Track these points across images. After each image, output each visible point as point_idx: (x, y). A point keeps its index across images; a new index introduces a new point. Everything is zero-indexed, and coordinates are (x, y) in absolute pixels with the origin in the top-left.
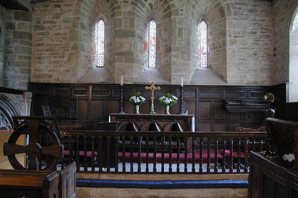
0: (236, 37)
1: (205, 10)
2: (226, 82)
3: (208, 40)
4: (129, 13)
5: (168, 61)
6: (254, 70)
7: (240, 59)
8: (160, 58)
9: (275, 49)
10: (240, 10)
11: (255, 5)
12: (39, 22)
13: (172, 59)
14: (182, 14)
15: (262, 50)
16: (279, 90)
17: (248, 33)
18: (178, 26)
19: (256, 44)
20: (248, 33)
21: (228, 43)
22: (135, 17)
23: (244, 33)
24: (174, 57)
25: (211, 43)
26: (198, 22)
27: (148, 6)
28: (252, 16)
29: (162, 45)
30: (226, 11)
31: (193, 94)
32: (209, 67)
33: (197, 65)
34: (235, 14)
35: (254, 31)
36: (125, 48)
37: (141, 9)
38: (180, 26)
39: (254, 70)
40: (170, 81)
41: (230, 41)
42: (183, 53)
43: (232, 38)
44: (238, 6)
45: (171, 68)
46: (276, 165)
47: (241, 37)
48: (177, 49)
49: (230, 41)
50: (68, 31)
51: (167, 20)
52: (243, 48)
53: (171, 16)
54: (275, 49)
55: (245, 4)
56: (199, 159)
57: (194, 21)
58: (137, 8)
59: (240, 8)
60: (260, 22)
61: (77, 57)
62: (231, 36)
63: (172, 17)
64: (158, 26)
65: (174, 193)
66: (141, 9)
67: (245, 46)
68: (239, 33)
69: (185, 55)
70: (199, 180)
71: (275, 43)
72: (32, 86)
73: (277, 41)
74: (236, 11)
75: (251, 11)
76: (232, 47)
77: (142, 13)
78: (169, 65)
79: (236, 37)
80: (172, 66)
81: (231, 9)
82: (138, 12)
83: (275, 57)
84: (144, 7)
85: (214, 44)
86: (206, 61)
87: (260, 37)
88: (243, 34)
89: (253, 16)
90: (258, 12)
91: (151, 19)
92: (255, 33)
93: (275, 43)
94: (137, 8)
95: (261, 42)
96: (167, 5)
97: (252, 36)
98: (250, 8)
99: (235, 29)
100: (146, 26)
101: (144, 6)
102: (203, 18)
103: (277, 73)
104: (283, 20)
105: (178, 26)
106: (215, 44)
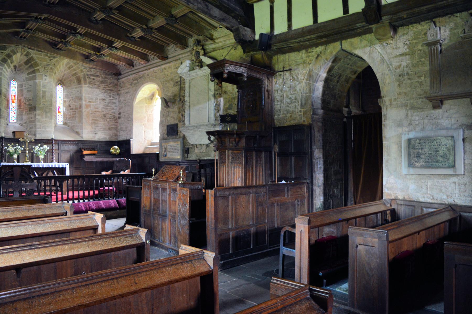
0: (90, 102)
1: (63, 76)
2: (82, 137)
3: (64, 102)
5: (32, 118)
6: (104, 129)
7: (93, 120)
8: (22, 115)
9: (120, 114)
10: (94, 81)
11: (106, 78)
13: (37, 117)
14: (45, 79)
15: (110, 113)
16: (125, 145)
17: (100, 100)
18: (42, 89)
19: (106, 109)
20: (100, 100)
21: (84, 106)
22: (2, 77)
24: (39, 115)
25: (67, 104)
26: (56, 86)
27: (12, 67)
28: (103, 86)
29: (25, 103)
30: (82, 80)
32: (65, 124)
33: (54, 125)
34: (90, 83)
35: (104, 98)
37: (7, 70)
38: (44, 90)
39: (104, 129)
40: (35, 135)
41: (86, 105)
42: (46, 112)
43: (87, 103)
44: (92, 77)
45: (35, 125)
46: (249, 255)
47: (94, 102)
48: (41, 109)
49: (86, 105)
51: (31, 82)
52: (96, 111)
53: (36, 79)
54: (120, 114)
55: (97, 76)
58: (4, 69)
59: (94, 79)
60: (109, 91)
62: (86, 101)
63: (37, 81)
65: (3, 215)
66: (7, 70)
67: (97, 110)
68: (92, 99)
69: (49, 115)
71: (120, 109)
73: (122, 107)
74: (91, 81)
75: (102, 82)
76: (87, 110)
77: (7, 73)
78: (34, 121)
79: (90, 102)
80: (37, 123)
81: (87, 79)
82: (4, 72)
83: (120, 119)
84: (9, 68)
85: (70, 106)
86: (62, 119)
87: (109, 103)
88: (96, 100)
89: (104, 86)
90: (107, 83)
92: (103, 100)
93: (120, 109)
94: (4, 69)
95: (109, 107)
96: (32, 70)
97: (102, 102)
98: (101, 79)
99: (90, 96)
100: (9, 85)
101: (9, 67)
102: (61, 82)
103: (122, 132)
104: (127, 93)
105: (42, 89)
106: (71, 105)
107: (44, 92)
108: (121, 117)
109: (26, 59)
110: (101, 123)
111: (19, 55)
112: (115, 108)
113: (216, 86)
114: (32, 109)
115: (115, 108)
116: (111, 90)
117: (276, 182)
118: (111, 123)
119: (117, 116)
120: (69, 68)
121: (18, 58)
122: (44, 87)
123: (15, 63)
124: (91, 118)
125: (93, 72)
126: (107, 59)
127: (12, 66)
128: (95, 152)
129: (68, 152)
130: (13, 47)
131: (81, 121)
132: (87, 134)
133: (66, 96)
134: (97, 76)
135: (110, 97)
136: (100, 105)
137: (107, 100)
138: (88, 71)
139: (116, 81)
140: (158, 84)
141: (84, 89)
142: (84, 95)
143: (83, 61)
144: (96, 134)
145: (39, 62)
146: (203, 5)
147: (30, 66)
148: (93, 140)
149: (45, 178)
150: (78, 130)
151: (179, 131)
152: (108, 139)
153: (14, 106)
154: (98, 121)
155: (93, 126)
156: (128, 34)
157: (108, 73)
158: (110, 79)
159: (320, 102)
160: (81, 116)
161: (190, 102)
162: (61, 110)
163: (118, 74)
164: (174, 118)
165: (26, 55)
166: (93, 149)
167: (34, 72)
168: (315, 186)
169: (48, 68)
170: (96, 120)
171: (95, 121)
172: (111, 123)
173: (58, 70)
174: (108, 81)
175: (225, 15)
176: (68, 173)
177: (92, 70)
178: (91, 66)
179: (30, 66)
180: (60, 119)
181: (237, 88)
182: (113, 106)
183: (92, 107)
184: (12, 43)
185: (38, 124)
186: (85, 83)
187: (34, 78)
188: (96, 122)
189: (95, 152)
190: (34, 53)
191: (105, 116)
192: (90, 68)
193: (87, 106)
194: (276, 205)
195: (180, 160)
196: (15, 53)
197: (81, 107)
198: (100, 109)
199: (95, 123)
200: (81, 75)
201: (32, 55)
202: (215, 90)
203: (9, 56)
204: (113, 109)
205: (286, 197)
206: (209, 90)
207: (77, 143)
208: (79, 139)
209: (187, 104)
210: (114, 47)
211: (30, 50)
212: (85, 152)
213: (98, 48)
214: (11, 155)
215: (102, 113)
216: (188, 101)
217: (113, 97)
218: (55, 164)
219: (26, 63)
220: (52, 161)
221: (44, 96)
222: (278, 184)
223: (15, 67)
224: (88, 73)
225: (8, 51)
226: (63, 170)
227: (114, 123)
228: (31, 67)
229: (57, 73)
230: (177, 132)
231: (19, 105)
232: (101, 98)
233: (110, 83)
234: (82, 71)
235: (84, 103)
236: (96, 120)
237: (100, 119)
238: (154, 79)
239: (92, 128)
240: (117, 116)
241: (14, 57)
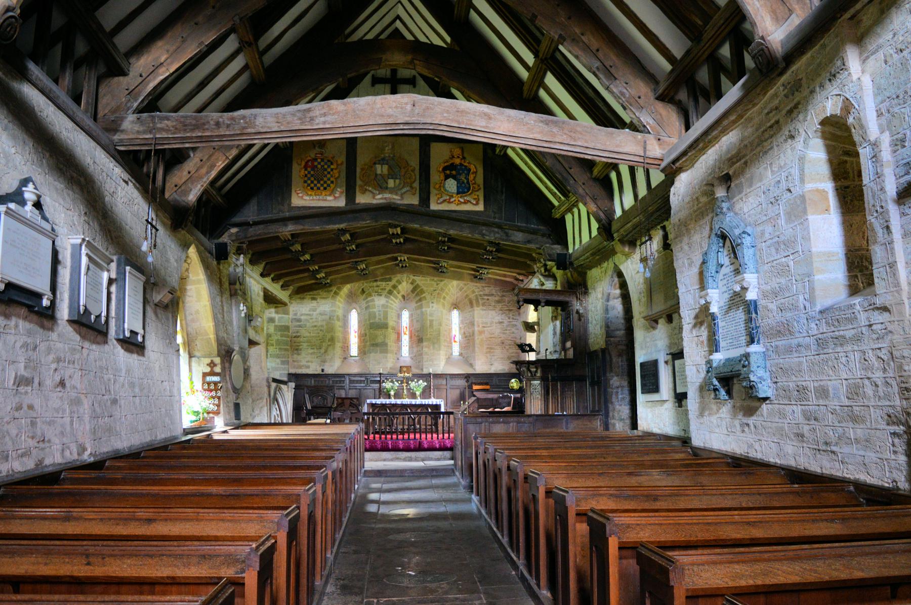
3: (460, 328)
4: (383, 305)
12: (296, 314)
18: (429, 318)
21: (476, 333)
23: (492, 323)
26: (450, 311)
28: (499, 306)
30: (474, 302)
31: (444, 382)
32: (461, 354)
33: (447, 359)
34: (483, 305)
36: (380, 340)
42: (434, 344)
43: (480, 329)
48: (429, 340)
50: (324, 323)
51: (419, 312)
56: (755, 394)
57: (445, 311)
61: (334, 349)
64: (411, 316)
68: (486, 323)
69: (436, 346)
70: (459, 267)
72: (293, 377)
75: (499, 302)
76: (481, 337)
78: (421, 354)
87: (507, 326)
91: (402, 309)
92: (501, 323)
98: (497, 298)
100: (399, 316)
101: (396, 297)
102: (455, 306)
105: (429, 318)
107: (431, 321)
109: (411, 287)
110: (498, 351)
111: (404, 284)
112: (516, 331)
114: (420, 340)
115: (516, 331)
116: (510, 310)
117: (368, 401)
118: (511, 351)
120: (461, 290)
121: (405, 287)
122: (431, 315)
123: (402, 293)
124: (485, 347)
125: (487, 291)
127: (400, 296)
128: (488, 387)
129: (457, 387)
130: (399, 276)
131: (474, 351)
132: (481, 366)
133: (462, 322)
136: (497, 330)
137: (506, 323)
141: (476, 312)
142: (476, 319)
143: (472, 281)
145: (425, 289)
146: (502, 234)
147: (417, 292)
149: (394, 414)
150: (472, 362)
152: (506, 371)
153: (405, 339)
159: (623, 321)
160: (474, 344)
162: (457, 339)
165: (412, 283)
166: (487, 384)
167: (420, 300)
169: (435, 293)
170: (491, 348)
171: (490, 350)
172: (511, 351)
173: (447, 294)
174: (507, 299)
175: (530, 237)
176: (443, 410)
179: (417, 292)
180: (456, 349)
182: (513, 330)
184: (394, 273)
185: (425, 357)
186: (478, 305)
187: (421, 307)
189: (488, 387)
190: (419, 280)
193: (481, 333)
196: (400, 283)
197: (473, 334)
198: (496, 334)
200: (472, 296)
201: (418, 282)
203: (395, 287)
207: (467, 377)
208: (471, 371)
211: (415, 278)
212: (475, 387)
214: (388, 391)
218: (433, 401)
219: (413, 291)
220: (430, 398)
221: (431, 326)
223: (403, 297)
225: (394, 282)
226: (437, 407)
228: (417, 295)
229: (447, 297)
231: (411, 337)
233: (509, 302)
234: (473, 292)
235: (476, 329)
236: (491, 348)
241: (400, 287)
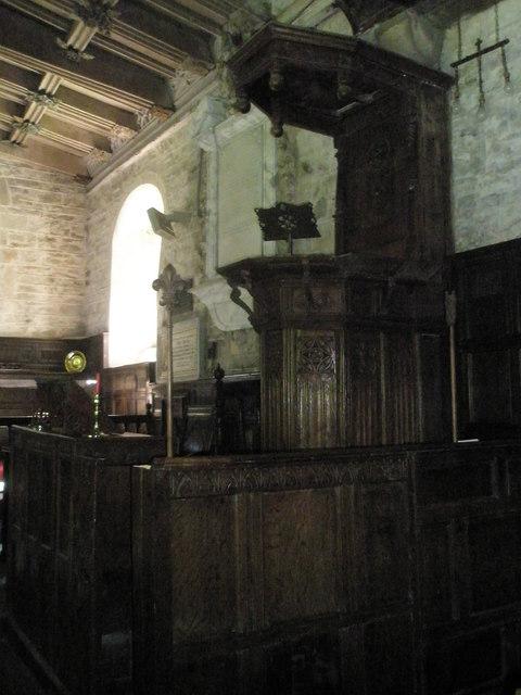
0: (15, 245)
7: (21, 287)
11: (57, 189)
15: (66, 272)
16: (91, 345)
28: (47, 208)
35: (50, 236)
47: (25, 246)
52: (28, 268)
54: (88, 274)
67: (32, 264)
75: (46, 199)
79: (15, 245)
90: (59, 200)
95: (63, 259)
97: (46, 246)
98: (44, 191)
99: (16, 231)
108: (88, 277)
113: (280, 152)
115: (78, 259)
118: (69, 296)
119: (82, 279)
124: (16, 285)
125: (24, 174)
126: (44, 135)
134: (37, 184)
135: (67, 232)
138: (12, 172)
139: (81, 198)
140: (157, 185)
144: (28, 321)
148: (22, 336)
151: (195, 300)
154: (34, 290)
155: (22, 302)
156: (59, 41)
157: (62, 177)
158: (69, 192)
161: (217, 214)
163: (85, 179)
164: (185, 265)
168: (25, 330)
177: (23, 169)
178: (18, 160)
181: (336, 146)
183: (19, 256)
188: (30, 294)
191: (52, 280)
192: (16, 165)
194: (450, 527)
195: (196, 378)
199: (26, 296)
202: (279, 166)
204: (72, 262)
205: (496, 495)
206: (264, 167)
209: (212, 218)
210: (43, 92)
213: (17, 105)
215: (47, 273)
216: (214, 211)
217: (73, 235)
222: (458, 445)
224: (12, 176)
227: (75, 297)
230: (192, 302)
232: (42, 235)
236: (29, 289)
237: (39, 287)
238: (151, 173)
239: (20, 307)
240: (82, 279)
